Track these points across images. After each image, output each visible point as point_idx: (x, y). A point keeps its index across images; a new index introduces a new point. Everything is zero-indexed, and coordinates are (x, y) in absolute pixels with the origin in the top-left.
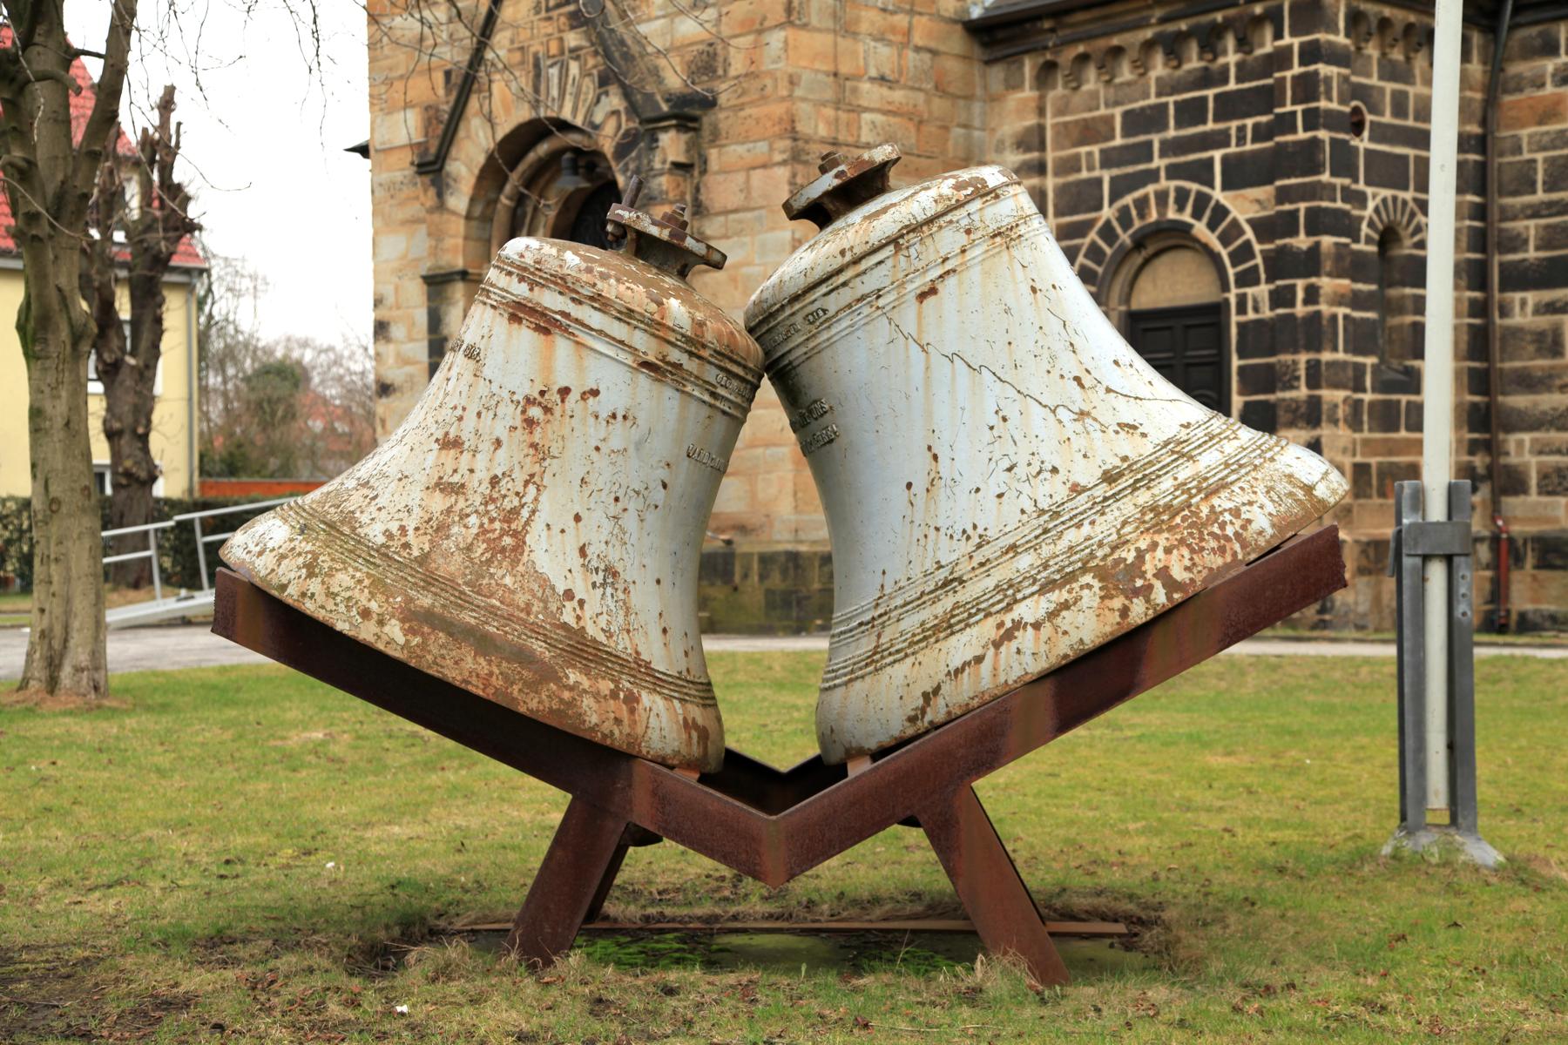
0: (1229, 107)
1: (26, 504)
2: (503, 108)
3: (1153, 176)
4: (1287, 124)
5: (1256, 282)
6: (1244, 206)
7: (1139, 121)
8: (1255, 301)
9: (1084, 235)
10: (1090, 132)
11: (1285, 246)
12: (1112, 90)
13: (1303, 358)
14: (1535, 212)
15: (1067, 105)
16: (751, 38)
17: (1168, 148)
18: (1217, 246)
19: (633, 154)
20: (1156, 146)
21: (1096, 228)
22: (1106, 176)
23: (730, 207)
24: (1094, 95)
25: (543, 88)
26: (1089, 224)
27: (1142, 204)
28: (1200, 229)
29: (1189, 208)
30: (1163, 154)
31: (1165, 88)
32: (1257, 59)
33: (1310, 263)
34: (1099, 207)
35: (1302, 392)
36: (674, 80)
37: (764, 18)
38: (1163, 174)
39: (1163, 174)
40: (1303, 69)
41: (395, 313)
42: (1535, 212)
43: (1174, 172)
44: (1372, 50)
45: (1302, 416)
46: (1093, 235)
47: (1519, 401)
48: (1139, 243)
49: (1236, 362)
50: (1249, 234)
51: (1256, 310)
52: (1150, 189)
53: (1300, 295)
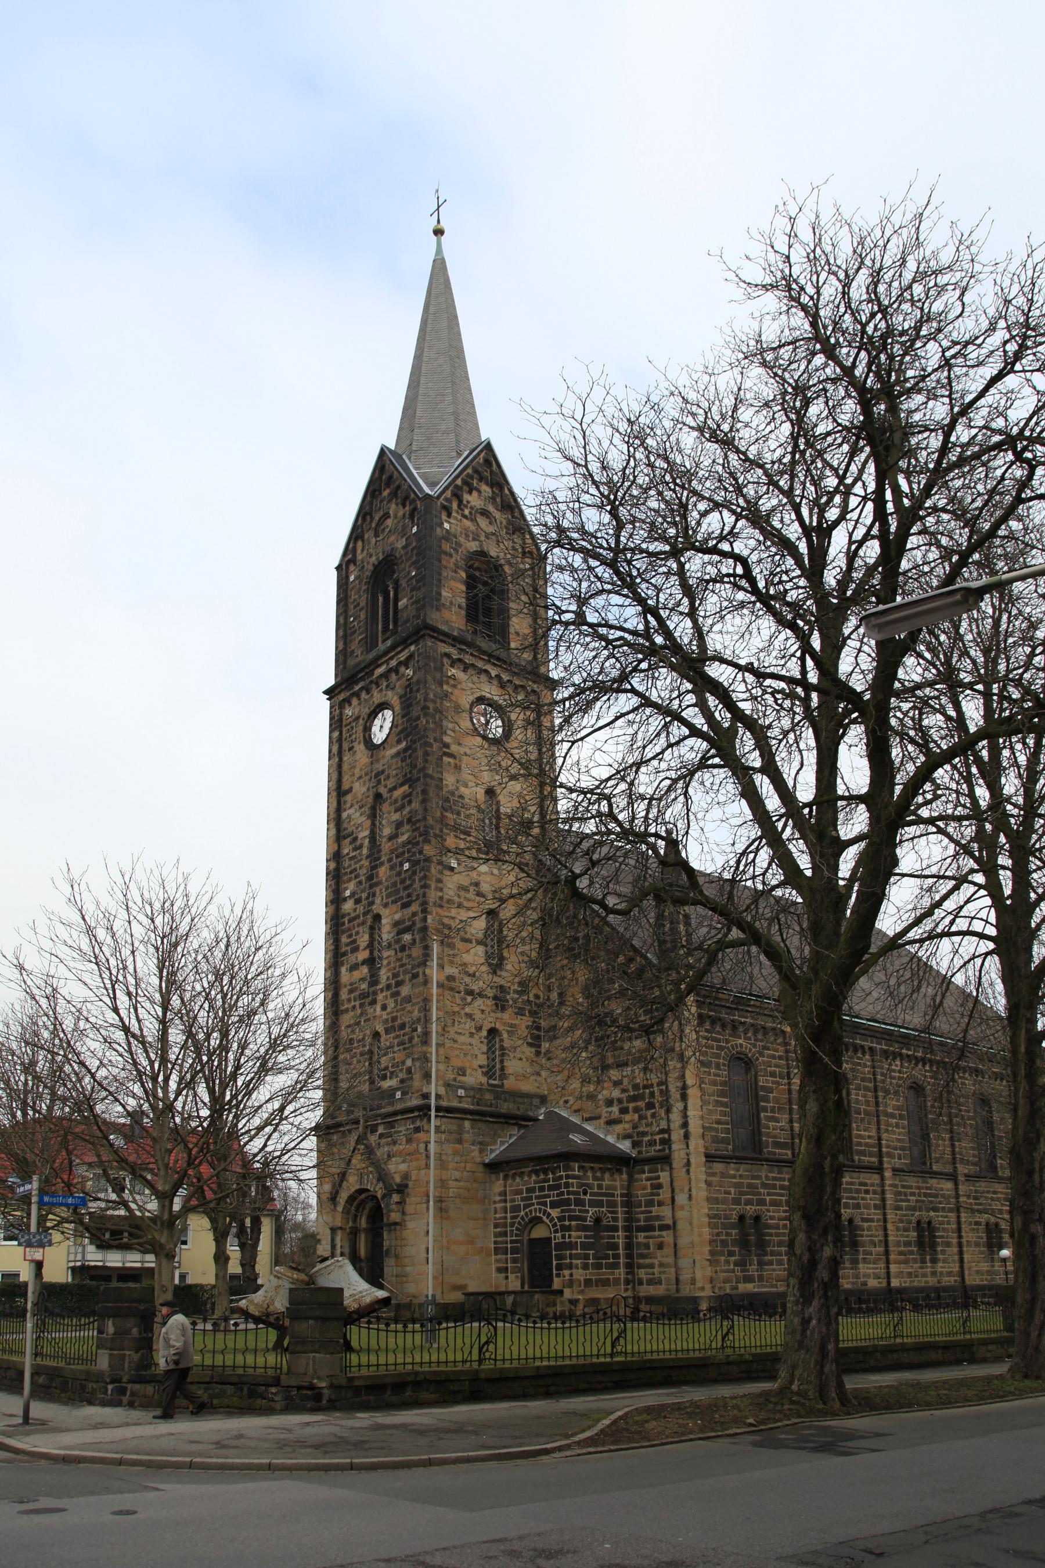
1: (214, 1287)
2: (352, 1183)
4: (562, 1193)
6: (555, 1213)
7: (529, 1190)
10: (518, 1192)
14: (642, 1212)
17: (537, 1197)
31: (536, 1182)
33: (569, 1228)
36: (398, 1180)
42: (642, 1212)
44: (590, 1174)
48: (531, 1221)
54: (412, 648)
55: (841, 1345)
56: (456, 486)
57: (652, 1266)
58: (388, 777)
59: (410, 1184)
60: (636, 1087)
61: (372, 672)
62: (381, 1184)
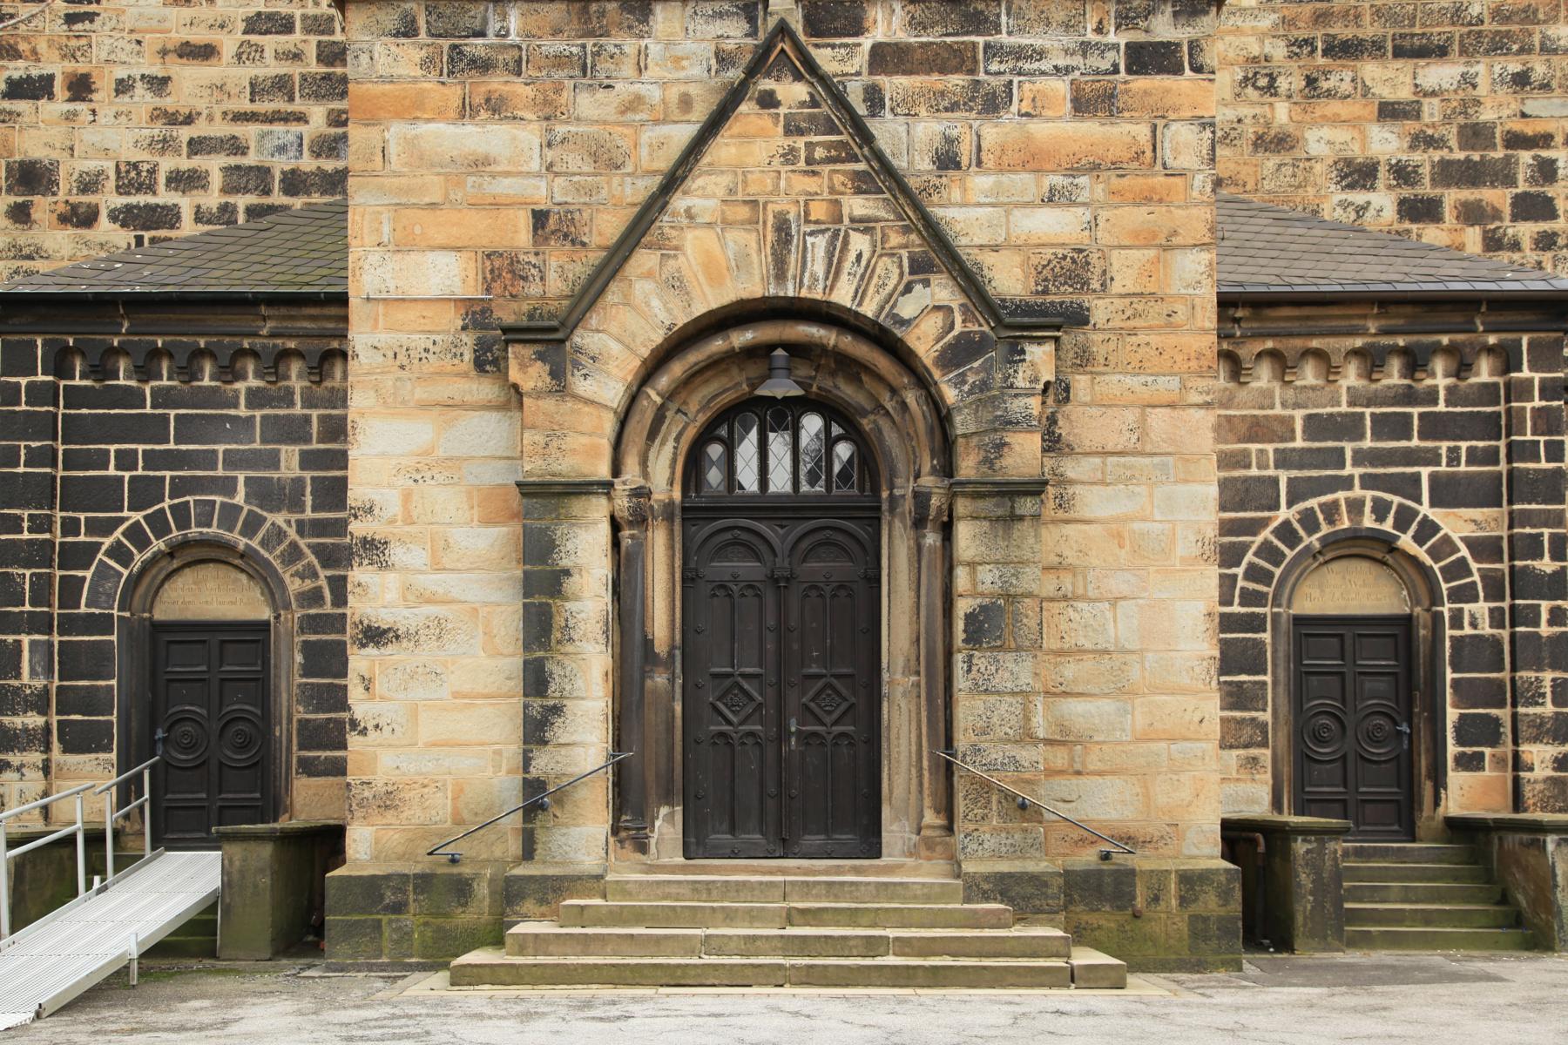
0: (1435, 427)
3: (1347, 483)
5: (1475, 599)
8: (1473, 617)
9: (1255, 534)
11: (1527, 567)
12: (1291, 392)
15: (1231, 399)
16: (1152, 253)
18: (1428, 561)
19: (976, 365)
20: (1348, 455)
21: (1271, 528)
22: (1284, 477)
23: (1109, 448)
24: (1268, 394)
25: (793, 259)
26: (1264, 523)
27: (1331, 511)
28: (1406, 541)
29: (1390, 520)
30: (1355, 463)
32: (1471, 386)
34: (1276, 507)
37: (1175, 233)
38: (1357, 482)
39: (1357, 482)
40: (1544, 403)
41: (400, 529)
43: (1369, 482)
45: (1548, 731)
46: (1266, 534)
49: (1450, 675)
50: (1464, 552)
51: (1474, 625)
52: (1341, 495)
53: (1544, 616)
55: (1300, 847)
59: (1101, 310)
60: (1476, 135)
62: (942, 290)
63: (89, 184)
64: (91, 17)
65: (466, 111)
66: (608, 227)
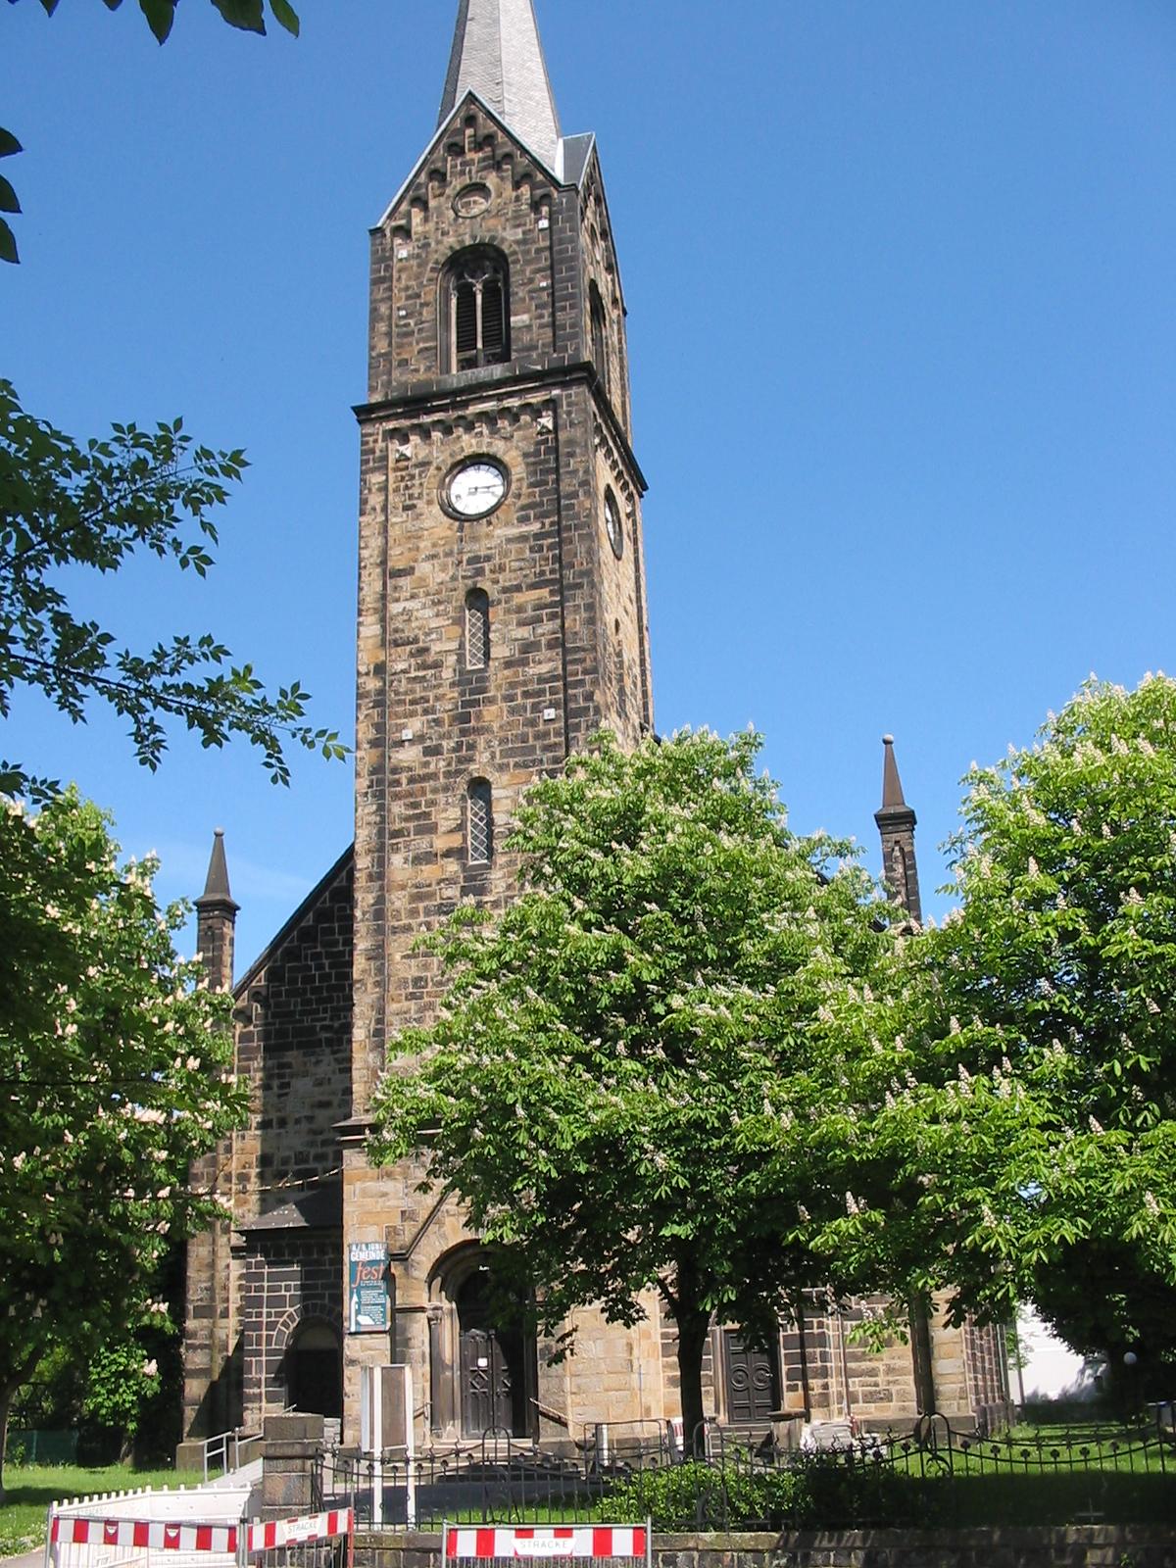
4: (550, 547)
13: (818, 1350)
35: (819, 1364)
47: (851, 1365)
49: (783, 1352)
54: (556, 392)
56: (419, 186)
57: (873, 1373)
58: (502, 569)
61: (465, 404)
63: (285, 1161)
64: (286, 1094)
65: (379, 1178)
66: (423, 1215)
